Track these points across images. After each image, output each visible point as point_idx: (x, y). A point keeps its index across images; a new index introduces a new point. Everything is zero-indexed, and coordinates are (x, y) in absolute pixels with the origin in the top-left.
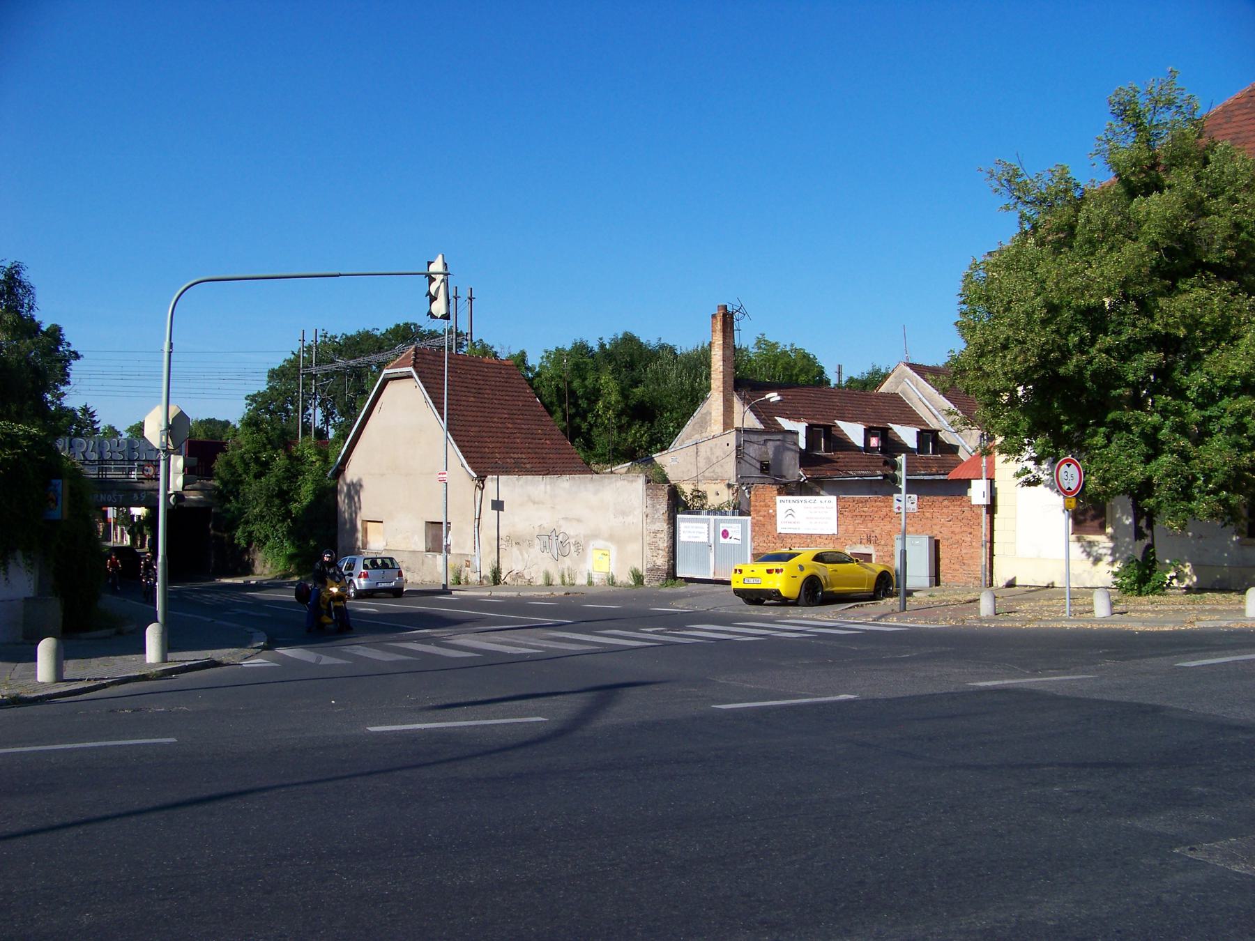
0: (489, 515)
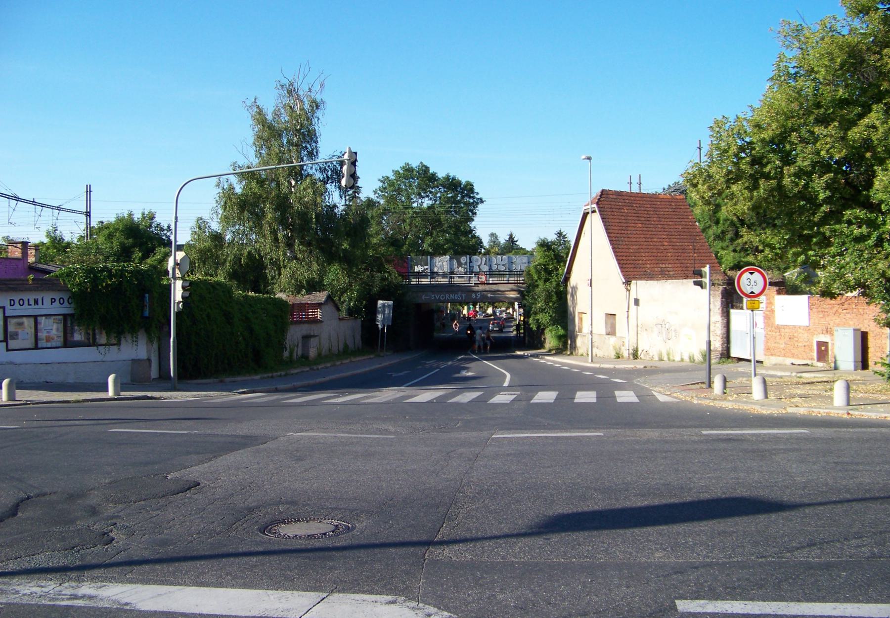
0: (633, 307)
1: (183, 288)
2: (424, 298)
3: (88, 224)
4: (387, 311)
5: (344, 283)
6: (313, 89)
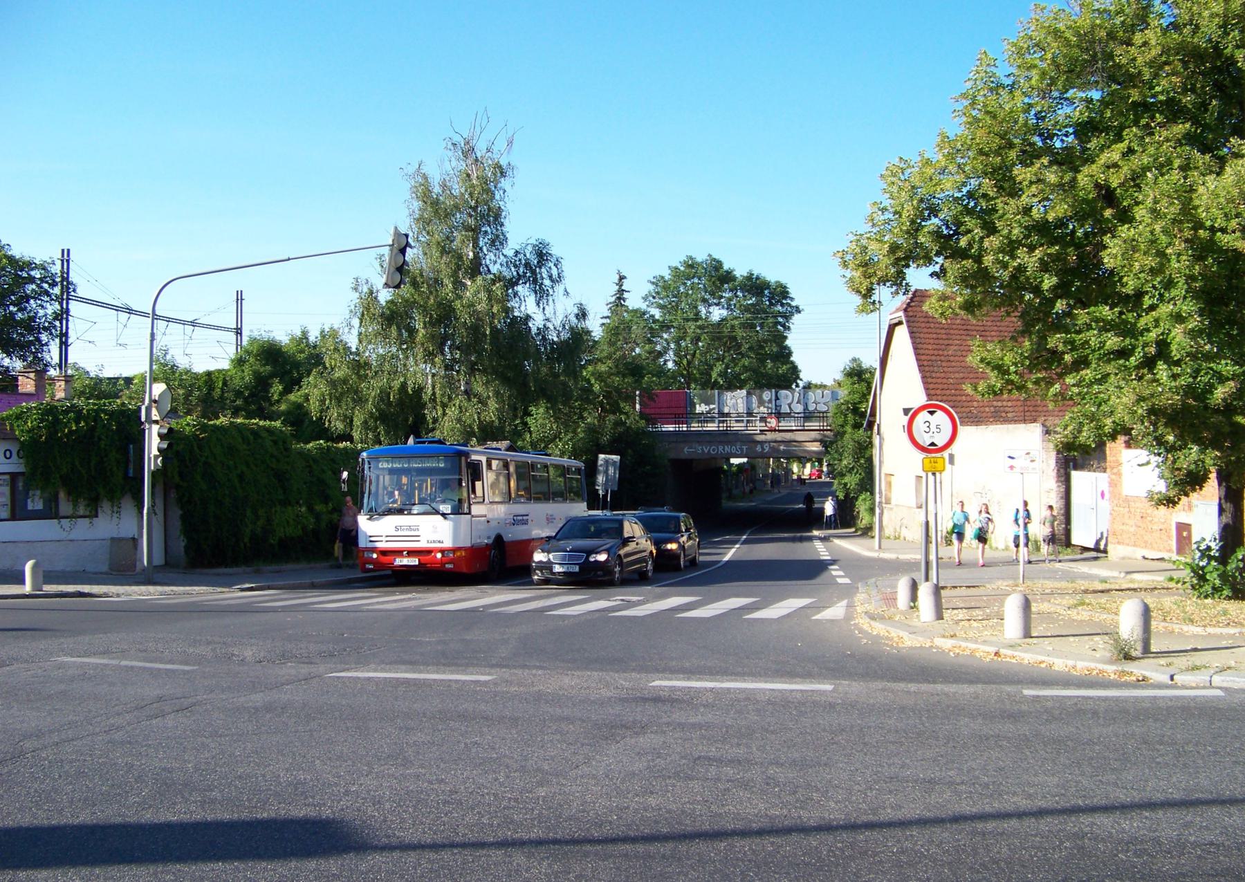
1: (161, 436)
2: (687, 451)
3: (238, 344)
4: (611, 471)
5: (551, 428)
6: (495, 149)
